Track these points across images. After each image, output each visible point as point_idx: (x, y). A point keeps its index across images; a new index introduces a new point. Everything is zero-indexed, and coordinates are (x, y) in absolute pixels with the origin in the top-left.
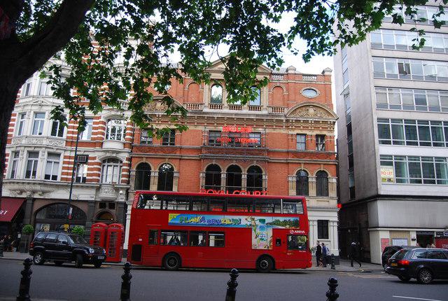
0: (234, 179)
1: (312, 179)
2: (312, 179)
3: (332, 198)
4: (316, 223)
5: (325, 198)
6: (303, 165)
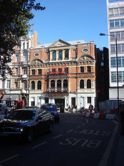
0: (59, 85)
1: (85, 83)
2: (85, 83)
3: (93, 89)
4: (87, 98)
5: (90, 89)
6: (33, 80)
